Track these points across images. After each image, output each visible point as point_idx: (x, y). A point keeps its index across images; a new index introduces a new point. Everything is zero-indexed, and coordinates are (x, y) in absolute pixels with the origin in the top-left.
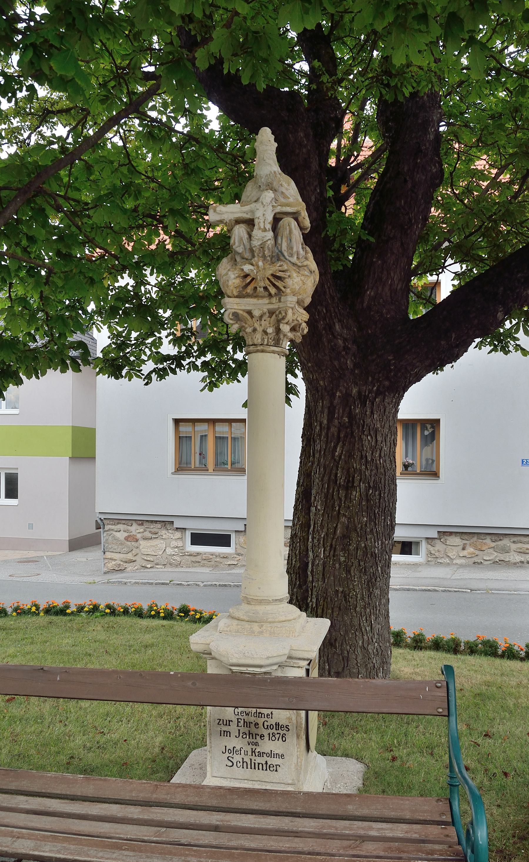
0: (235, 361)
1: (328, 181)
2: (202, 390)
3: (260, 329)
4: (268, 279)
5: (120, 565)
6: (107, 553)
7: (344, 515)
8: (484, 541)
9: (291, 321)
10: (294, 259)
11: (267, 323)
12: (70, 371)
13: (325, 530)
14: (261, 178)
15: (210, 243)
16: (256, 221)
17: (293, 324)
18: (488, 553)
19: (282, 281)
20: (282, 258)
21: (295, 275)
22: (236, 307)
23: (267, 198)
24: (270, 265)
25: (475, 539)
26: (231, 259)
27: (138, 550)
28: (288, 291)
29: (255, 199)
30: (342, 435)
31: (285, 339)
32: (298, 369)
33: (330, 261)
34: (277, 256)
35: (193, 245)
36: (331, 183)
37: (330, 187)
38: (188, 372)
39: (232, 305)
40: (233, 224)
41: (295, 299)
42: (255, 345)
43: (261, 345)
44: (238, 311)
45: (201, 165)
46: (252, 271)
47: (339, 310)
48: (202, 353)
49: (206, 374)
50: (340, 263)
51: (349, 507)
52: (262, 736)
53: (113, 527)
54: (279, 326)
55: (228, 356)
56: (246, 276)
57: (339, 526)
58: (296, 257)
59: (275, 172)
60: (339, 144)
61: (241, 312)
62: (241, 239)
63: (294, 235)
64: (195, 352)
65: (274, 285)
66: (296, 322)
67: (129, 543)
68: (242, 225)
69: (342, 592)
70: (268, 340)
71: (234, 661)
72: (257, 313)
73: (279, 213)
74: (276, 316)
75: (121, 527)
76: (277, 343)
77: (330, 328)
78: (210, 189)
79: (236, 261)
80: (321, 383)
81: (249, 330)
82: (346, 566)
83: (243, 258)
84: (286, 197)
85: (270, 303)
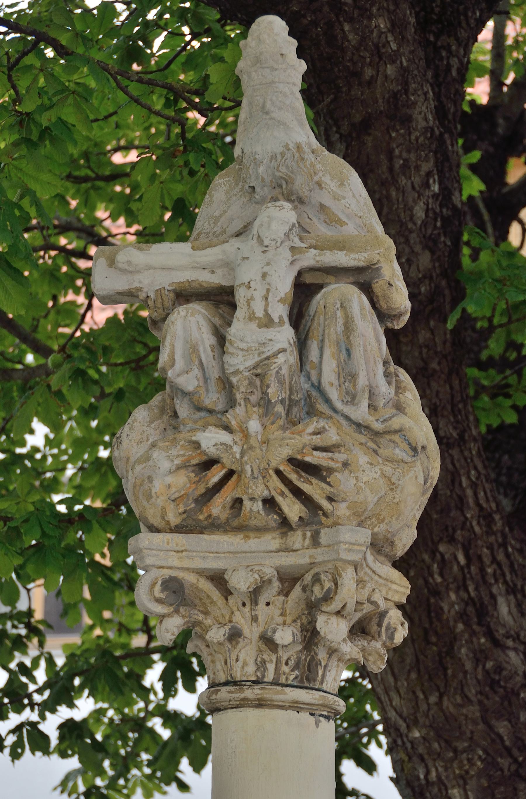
0: (171, 718)
1: (468, 149)
3: (251, 632)
4: (278, 473)
9: (351, 606)
10: (360, 412)
11: (274, 611)
14: (257, 163)
15: (94, 346)
16: (241, 295)
17: (357, 616)
19: (323, 479)
20: (322, 407)
22: (176, 563)
23: (274, 226)
24: (284, 428)
26: (162, 409)
28: (342, 510)
29: (237, 226)
31: (334, 662)
32: (379, 745)
33: (476, 397)
34: (308, 403)
35: (41, 350)
36: (475, 156)
37: (473, 168)
38: (15, 755)
39: (157, 555)
40: (168, 303)
41: (364, 536)
42: (235, 683)
43: (256, 682)
44: (180, 575)
45: (70, 115)
46: (227, 447)
47: (508, 555)
48: (61, 692)
49: (74, 763)
50: (508, 403)
54: (313, 622)
55: (147, 702)
56: (209, 464)
58: (365, 403)
59: (299, 147)
60: (499, 35)
61: (190, 578)
62: (193, 350)
63: (359, 335)
64: (40, 691)
65: (298, 493)
66: (367, 608)
68: (196, 306)
70: (277, 669)
72: (241, 581)
73: (312, 270)
74: (306, 592)
76: (308, 675)
77: (480, 612)
78: (99, 178)
79: (175, 415)
81: (217, 634)
83: (199, 408)
84: (332, 220)
85: (287, 550)
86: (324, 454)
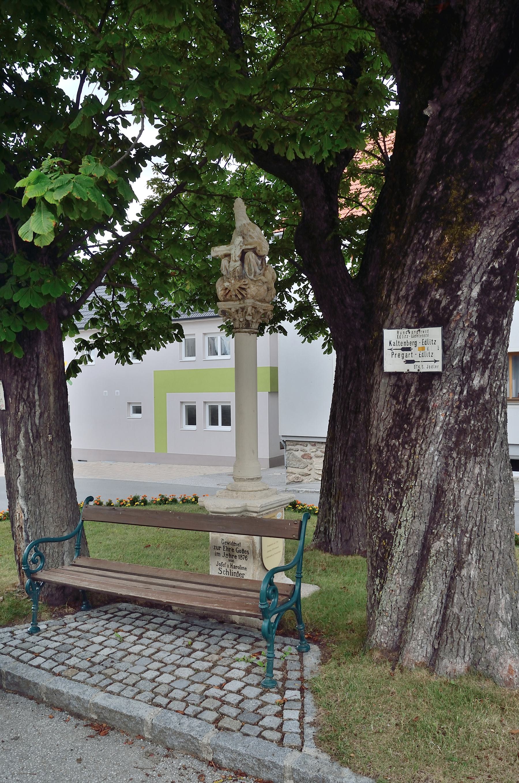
2: (303, 342)
5: (298, 477)
6: (288, 468)
7: (353, 432)
12: (175, 342)
13: (341, 442)
21: (252, 286)
27: (312, 466)
30: (353, 375)
51: (356, 426)
52: (236, 557)
53: (292, 447)
56: (226, 289)
57: (350, 439)
62: (225, 267)
67: (305, 460)
69: (351, 485)
71: (211, 510)
75: (298, 447)
80: (340, 339)
82: (354, 466)
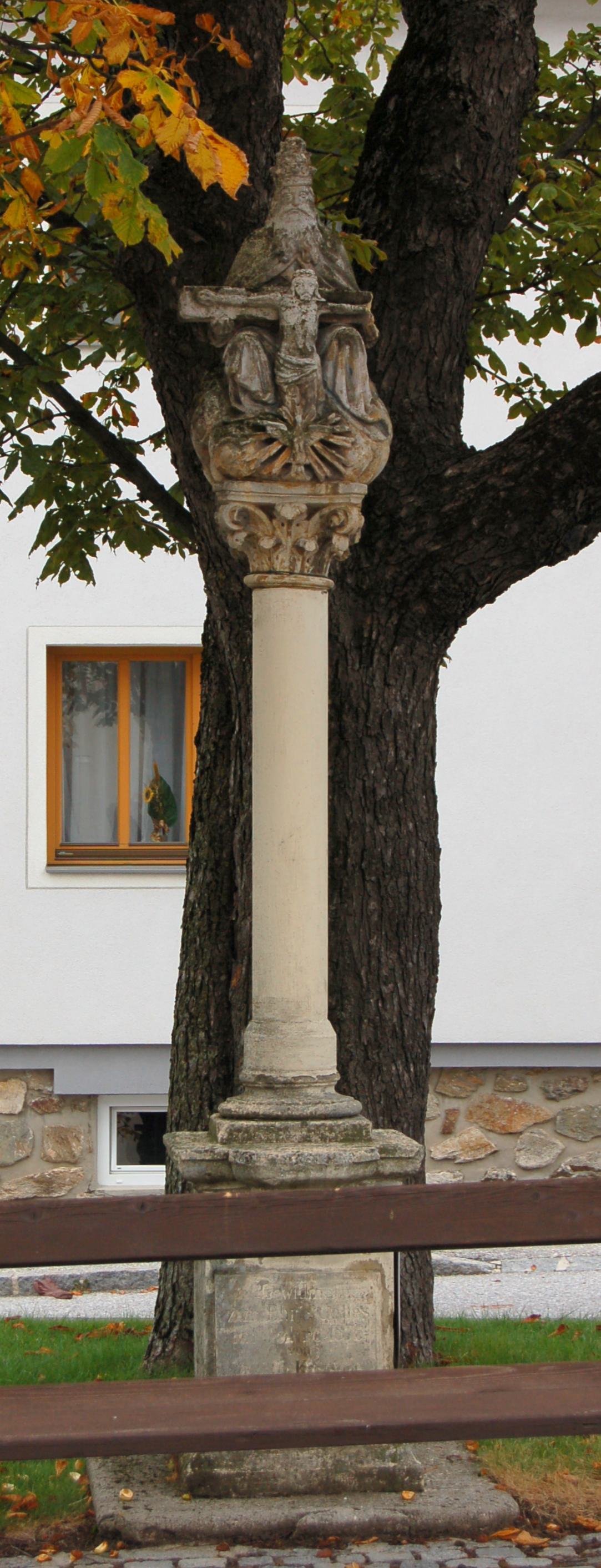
8: (519, 1099)
18: (533, 1142)
21: (362, 441)
22: (245, 499)
25: (487, 1090)
72: (288, 512)
86: (341, 437)
